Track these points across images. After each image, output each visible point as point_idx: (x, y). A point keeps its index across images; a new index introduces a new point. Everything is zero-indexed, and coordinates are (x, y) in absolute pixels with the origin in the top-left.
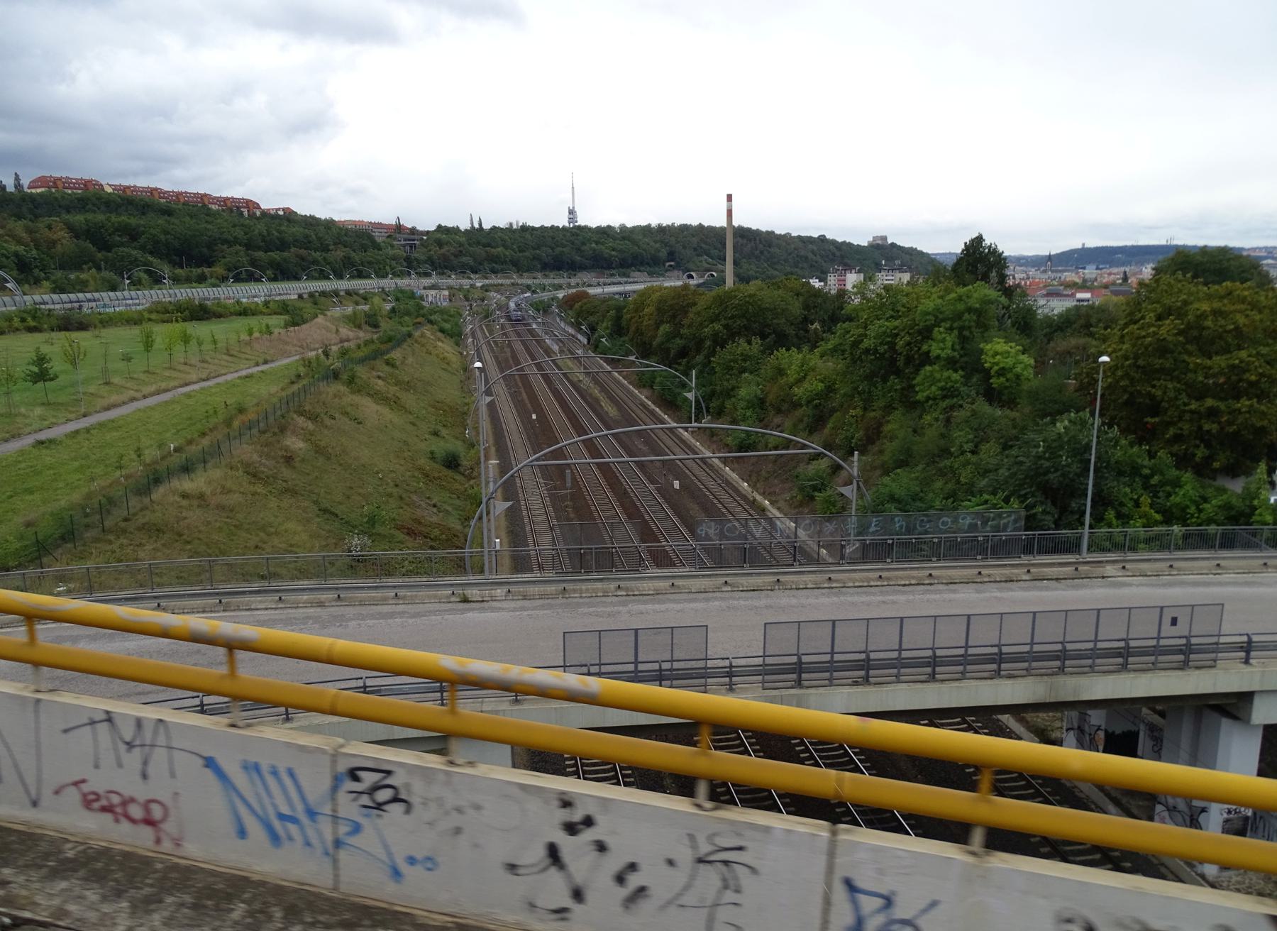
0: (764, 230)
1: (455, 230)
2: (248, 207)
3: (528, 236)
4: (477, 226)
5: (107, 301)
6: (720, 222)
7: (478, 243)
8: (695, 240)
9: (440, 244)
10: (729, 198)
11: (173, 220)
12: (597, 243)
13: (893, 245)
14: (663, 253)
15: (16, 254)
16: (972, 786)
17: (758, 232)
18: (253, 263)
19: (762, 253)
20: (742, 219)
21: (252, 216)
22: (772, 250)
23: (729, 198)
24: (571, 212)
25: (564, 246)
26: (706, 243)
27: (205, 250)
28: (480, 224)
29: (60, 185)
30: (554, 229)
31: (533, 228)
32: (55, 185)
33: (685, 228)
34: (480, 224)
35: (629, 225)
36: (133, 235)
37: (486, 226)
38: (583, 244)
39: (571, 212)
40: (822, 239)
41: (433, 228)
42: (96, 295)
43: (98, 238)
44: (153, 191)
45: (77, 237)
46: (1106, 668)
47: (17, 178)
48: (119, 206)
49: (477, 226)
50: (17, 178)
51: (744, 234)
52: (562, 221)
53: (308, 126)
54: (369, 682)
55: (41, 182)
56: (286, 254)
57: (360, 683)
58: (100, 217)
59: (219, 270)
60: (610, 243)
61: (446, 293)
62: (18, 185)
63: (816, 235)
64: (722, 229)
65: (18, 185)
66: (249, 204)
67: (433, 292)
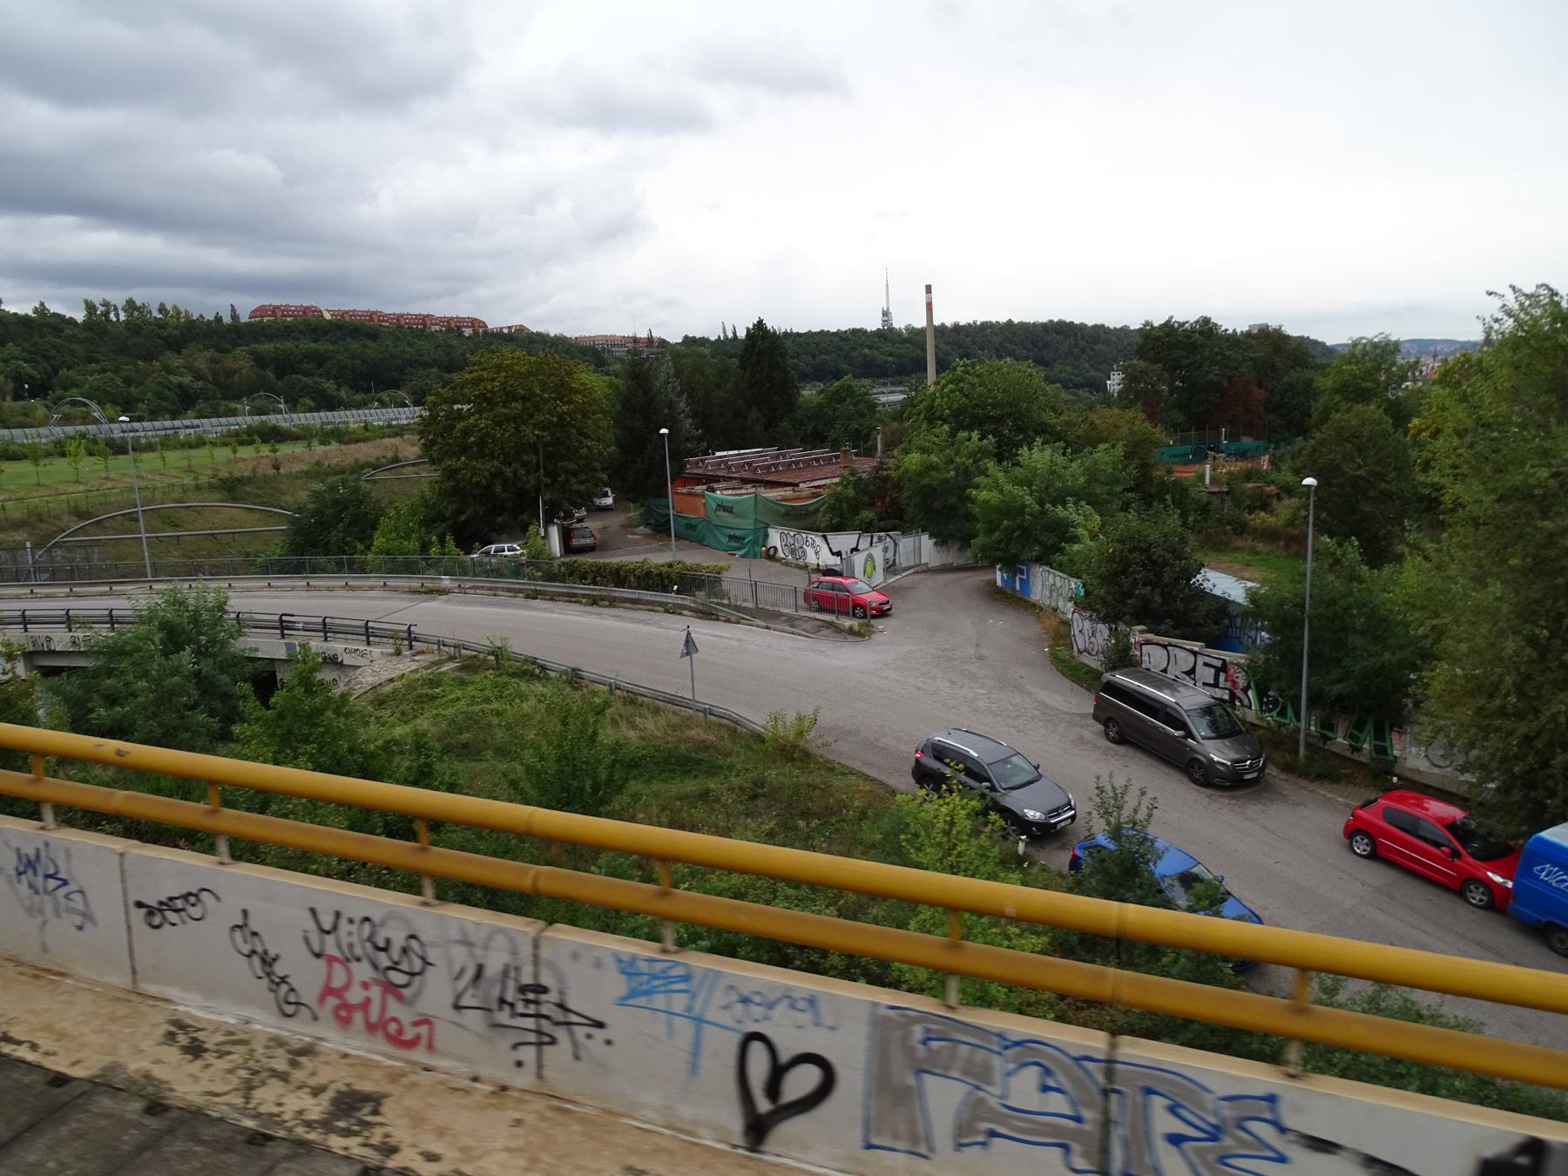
0: (1090, 324)
1: (703, 341)
2: (473, 326)
4: (730, 335)
5: (208, 428)
6: (920, 322)
8: (997, 339)
10: (929, 289)
11: (372, 345)
12: (870, 348)
16: (211, 849)
17: (1082, 327)
19: (1083, 350)
20: (946, 316)
22: (1097, 347)
23: (929, 289)
24: (886, 314)
25: (829, 353)
26: (1011, 342)
29: (279, 313)
30: (857, 333)
31: (799, 335)
32: (274, 314)
33: (986, 326)
35: (1016, 321)
36: (319, 360)
38: (854, 349)
39: (886, 314)
42: (196, 422)
43: (283, 366)
44: (371, 315)
46: (120, 800)
49: (730, 335)
51: (941, 331)
52: (873, 324)
53: (616, 230)
55: (260, 311)
58: (289, 345)
60: (887, 347)
62: (234, 316)
64: (922, 331)
65: (234, 316)
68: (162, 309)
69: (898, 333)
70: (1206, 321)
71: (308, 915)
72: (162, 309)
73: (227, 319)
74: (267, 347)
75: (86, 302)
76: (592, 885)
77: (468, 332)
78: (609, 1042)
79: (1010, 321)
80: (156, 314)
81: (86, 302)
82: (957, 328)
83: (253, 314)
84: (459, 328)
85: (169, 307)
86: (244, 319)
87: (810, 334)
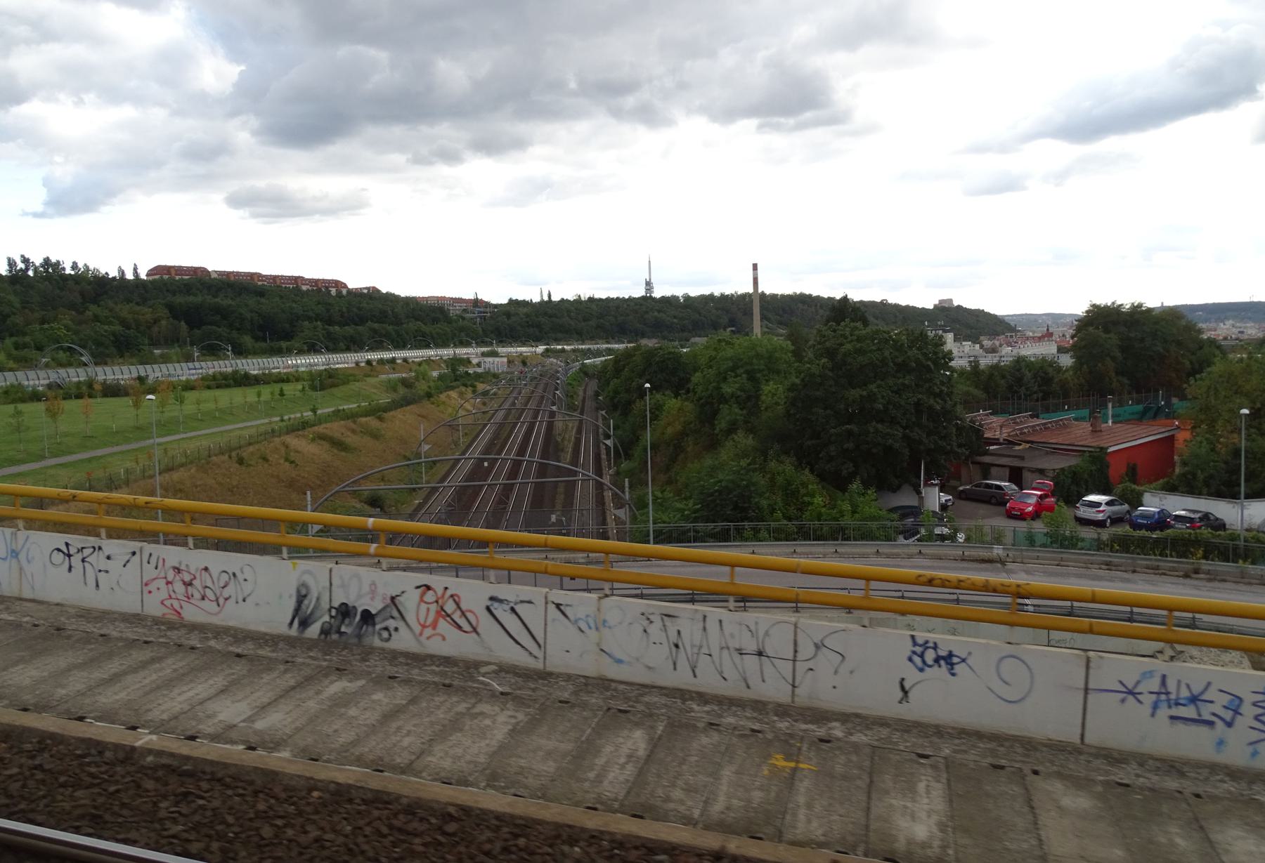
3: (594, 306)
6: (751, 290)
7: (546, 314)
9: (508, 315)
10: (755, 267)
11: (263, 300)
12: (659, 311)
13: (959, 307)
14: (725, 320)
15: (114, 334)
18: (329, 336)
20: (769, 286)
21: (339, 294)
23: (755, 267)
24: (648, 284)
27: (287, 326)
28: (549, 296)
29: (173, 272)
30: (631, 300)
34: (549, 296)
37: (555, 298)
39: (648, 284)
40: (477, 302)
41: (505, 301)
45: (175, 317)
46: (130, 523)
47: (135, 269)
48: (219, 289)
49: (546, 298)
50: (135, 269)
52: (639, 292)
54: (961, 597)
56: (360, 328)
57: (955, 597)
59: (296, 343)
61: (505, 360)
63: (879, 300)
66: (338, 284)
67: (490, 359)
68: (74, 266)
69: (654, 299)
70: (1094, 306)
71: (1205, 683)
72: (74, 266)
73: (130, 276)
74: (179, 299)
75: (9, 259)
76: (160, 525)
77: (333, 291)
78: (108, 558)
79: (845, 299)
80: (69, 271)
81: (9, 259)
82: (774, 296)
83: (151, 273)
84: (327, 288)
85: (81, 265)
86: (143, 276)
87: (609, 300)
